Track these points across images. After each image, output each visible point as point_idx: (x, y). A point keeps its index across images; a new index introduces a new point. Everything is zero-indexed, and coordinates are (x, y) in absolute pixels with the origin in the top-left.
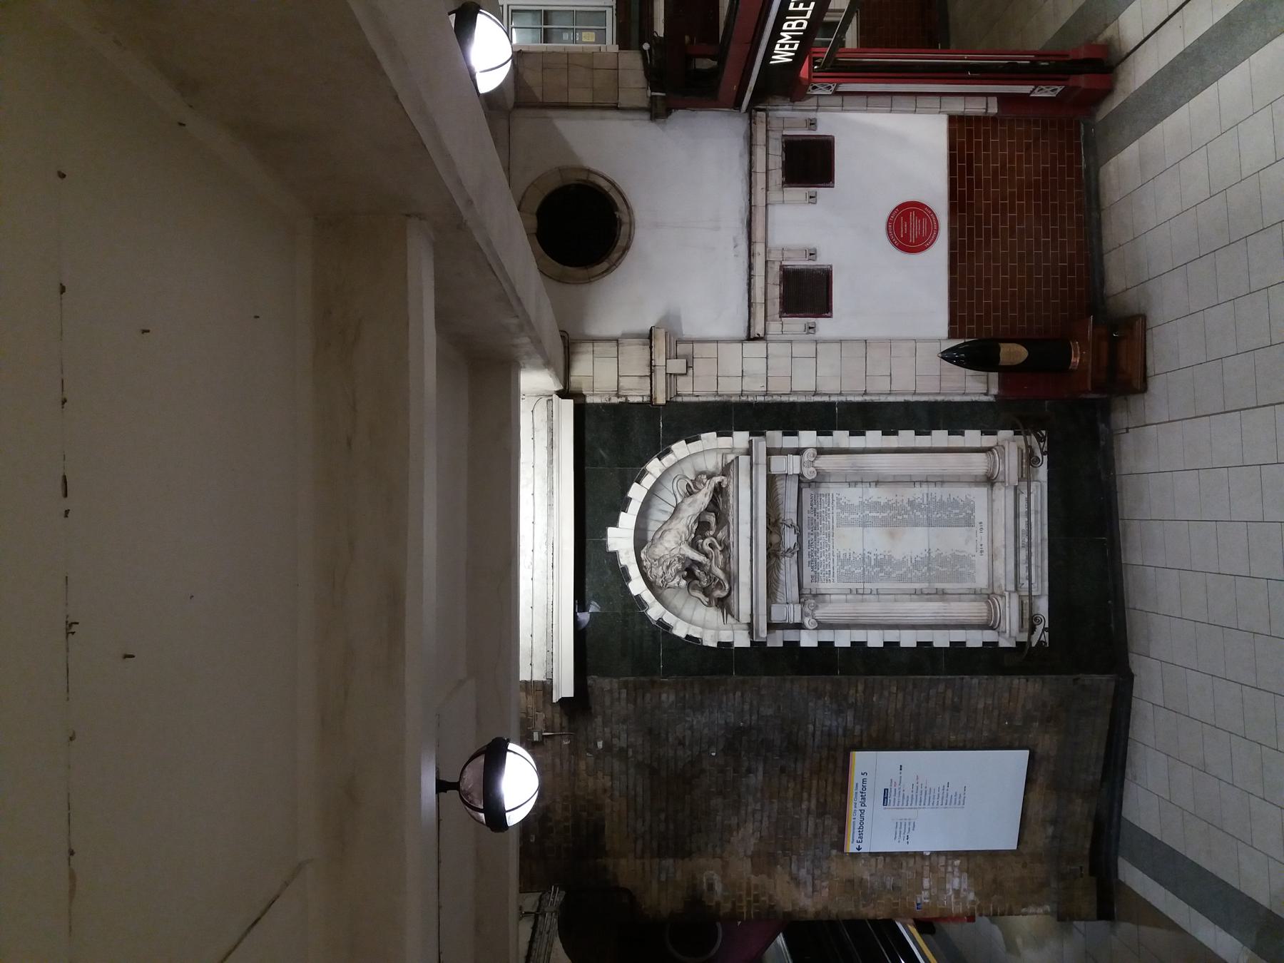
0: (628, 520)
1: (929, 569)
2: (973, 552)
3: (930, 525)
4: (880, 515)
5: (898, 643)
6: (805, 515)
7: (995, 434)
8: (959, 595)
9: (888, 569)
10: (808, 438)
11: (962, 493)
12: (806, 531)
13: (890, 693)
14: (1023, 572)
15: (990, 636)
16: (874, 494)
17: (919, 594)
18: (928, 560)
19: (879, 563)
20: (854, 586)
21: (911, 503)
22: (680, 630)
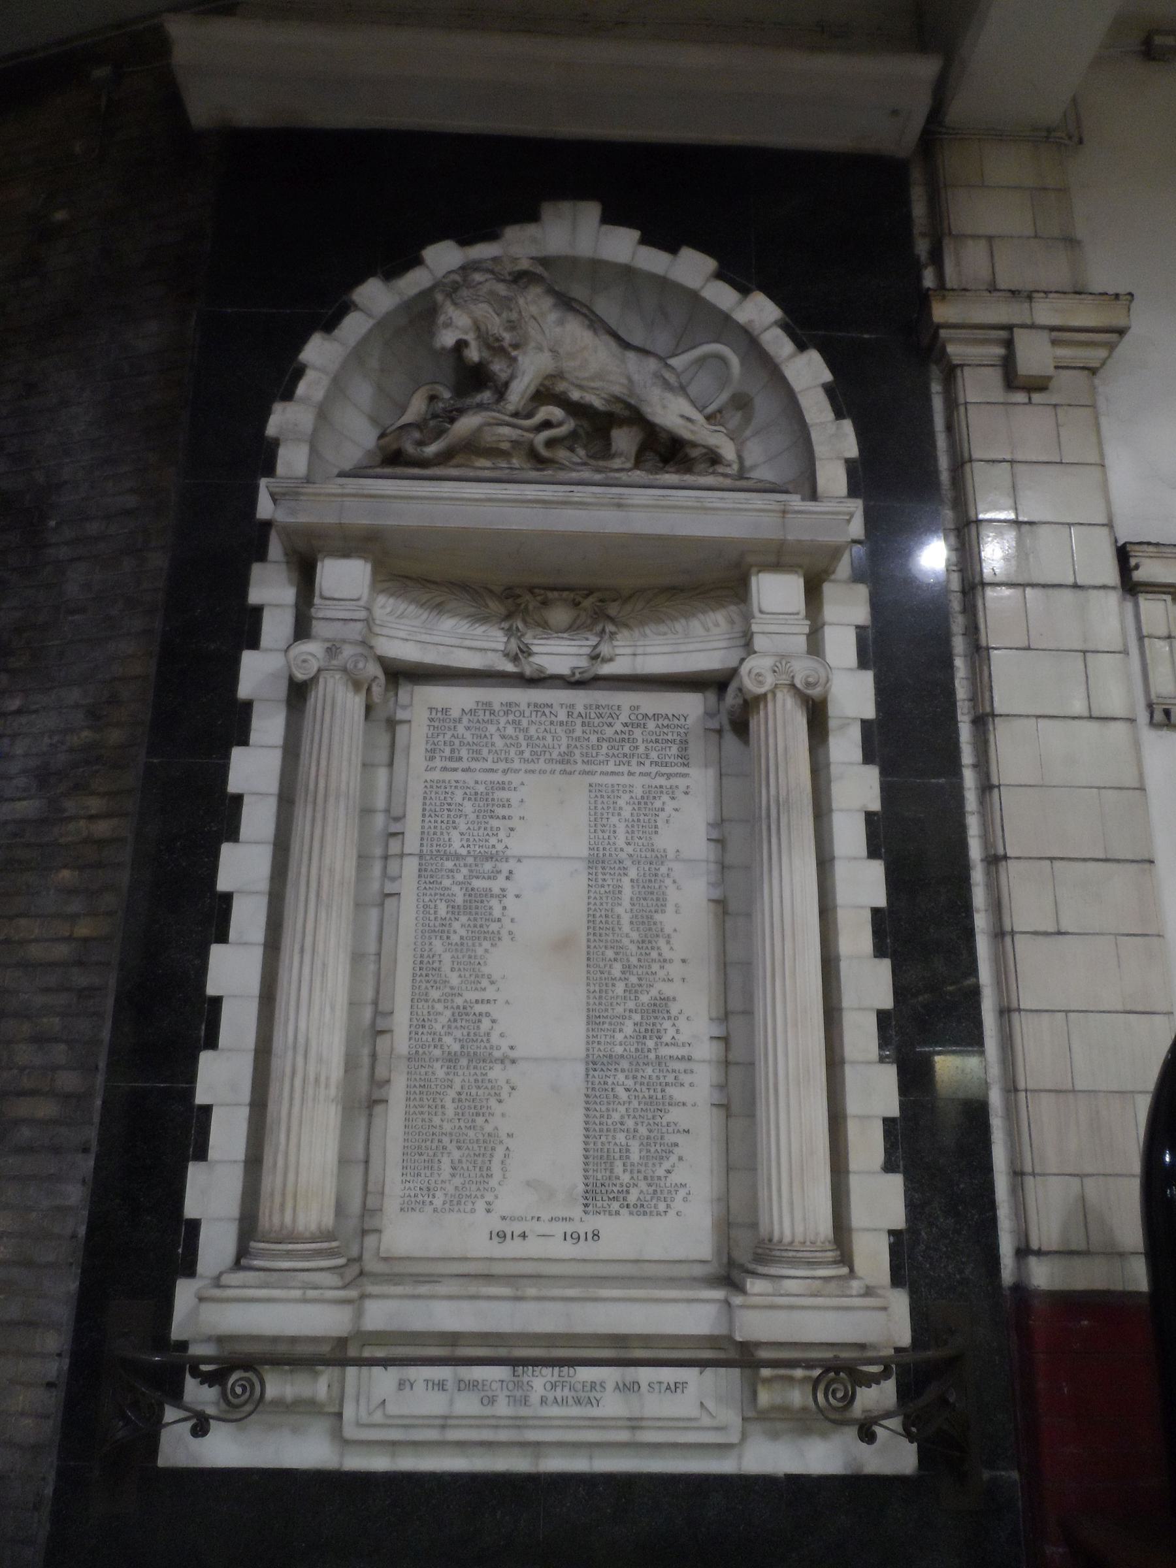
0: (621, 245)
1: (451, 1059)
2: (504, 1206)
3: (592, 1064)
4: (623, 911)
5: (223, 938)
8: (357, 1160)
9: (459, 929)
11: (695, 1173)
12: (580, 698)
13: (74, 918)
14: (318, 832)
15: (216, 1245)
16: (689, 900)
17: (368, 1030)
18: (478, 1055)
19: (476, 904)
20: (413, 826)
21: (661, 1006)
22: (319, 352)
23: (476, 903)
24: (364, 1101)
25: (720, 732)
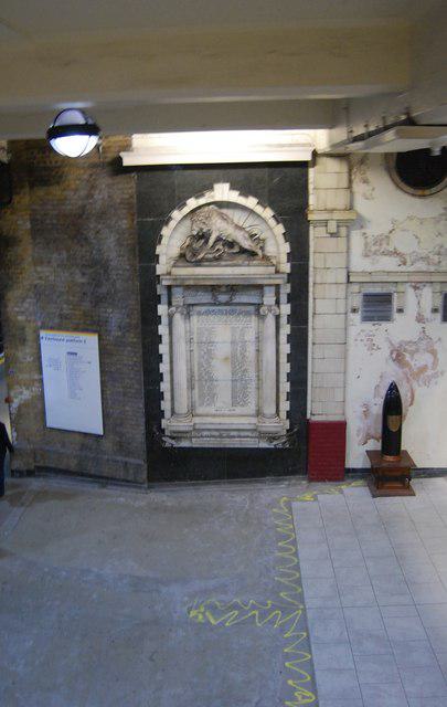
10: (286, 309)
15: (167, 414)
21: (246, 370)
23: (209, 352)
24: (191, 387)
25: (133, 215)
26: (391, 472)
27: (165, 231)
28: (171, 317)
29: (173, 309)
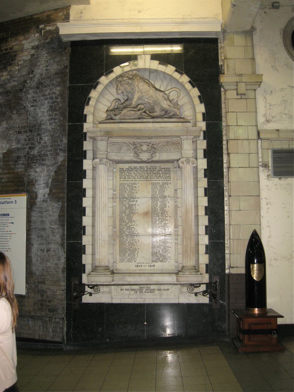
1: (127, 235)
2: (138, 261)
5: (85, 215)
6: (158, 165)
7: (207, 272)
9: (127, 212)
10: (203, 164)
12: (149, 165)
15: (88, 268)
23: (131, 206)
26: (126, 289)
27: (94, 94)
28: (94, 168)
29: (97, 160)
